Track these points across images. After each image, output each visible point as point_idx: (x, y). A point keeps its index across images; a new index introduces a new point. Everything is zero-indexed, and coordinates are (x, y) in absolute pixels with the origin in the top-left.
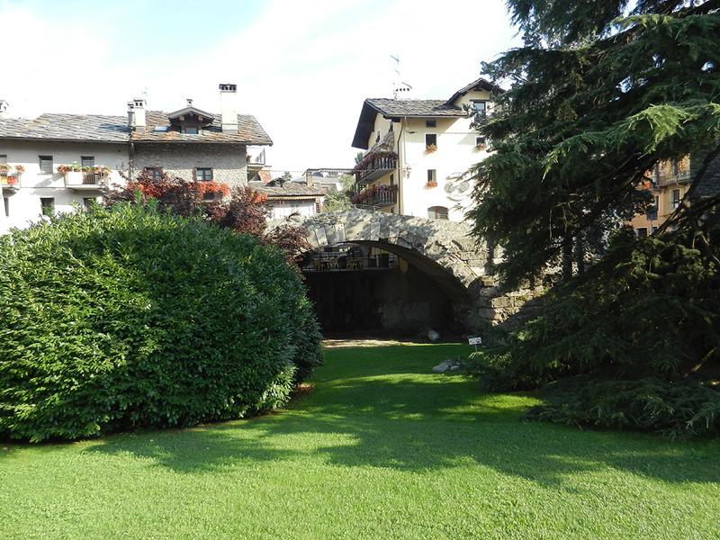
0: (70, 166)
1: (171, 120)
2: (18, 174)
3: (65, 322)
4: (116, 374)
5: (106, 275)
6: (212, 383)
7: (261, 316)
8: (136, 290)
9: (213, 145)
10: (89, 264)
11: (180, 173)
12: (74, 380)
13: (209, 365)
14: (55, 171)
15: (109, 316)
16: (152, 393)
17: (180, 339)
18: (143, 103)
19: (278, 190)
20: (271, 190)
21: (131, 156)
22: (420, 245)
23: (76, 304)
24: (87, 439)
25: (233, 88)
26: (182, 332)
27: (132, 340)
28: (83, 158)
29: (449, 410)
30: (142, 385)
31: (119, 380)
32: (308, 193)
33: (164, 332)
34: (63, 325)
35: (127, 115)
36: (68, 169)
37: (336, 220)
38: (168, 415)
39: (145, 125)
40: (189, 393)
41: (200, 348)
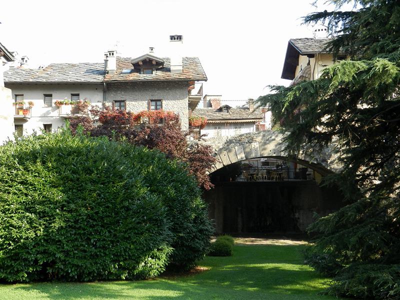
0: (62, 101)
1: (134, 65)
2: (30, 108)
3: (9, 205)
4: (37, 241)
5: (35, 176)
6: (100, 251)
7: (143, 208)
8: (53, 186)
9: (163, 82)
10: (26, 169)
11: (136, 106)
12: (11, 242)
13: (99, 240)
14: (53, 105)
15: (34, 202)
16: (58, 255)
17: (78, 220)
18: (115, 53)
19: (225, 115)
20: (219, 115)
21: (104, 92)
22: (325, 161)
23: (15, 194)
24: (20, 282)
25: (179, 38)
26: (80, 215)
27: (48, 219)
28: (73, 95)
29: (281, 287)
30: (52, 248)
31: (38, 244)
32: (250, 117)
33: (69, 215)
34: (7, 207)
35: (104, 62)
36: (61, 103)
37: (252, 139)
38: (70, 271)
39: (115, 69)
40: (85, 258)
41: (92, 226)
